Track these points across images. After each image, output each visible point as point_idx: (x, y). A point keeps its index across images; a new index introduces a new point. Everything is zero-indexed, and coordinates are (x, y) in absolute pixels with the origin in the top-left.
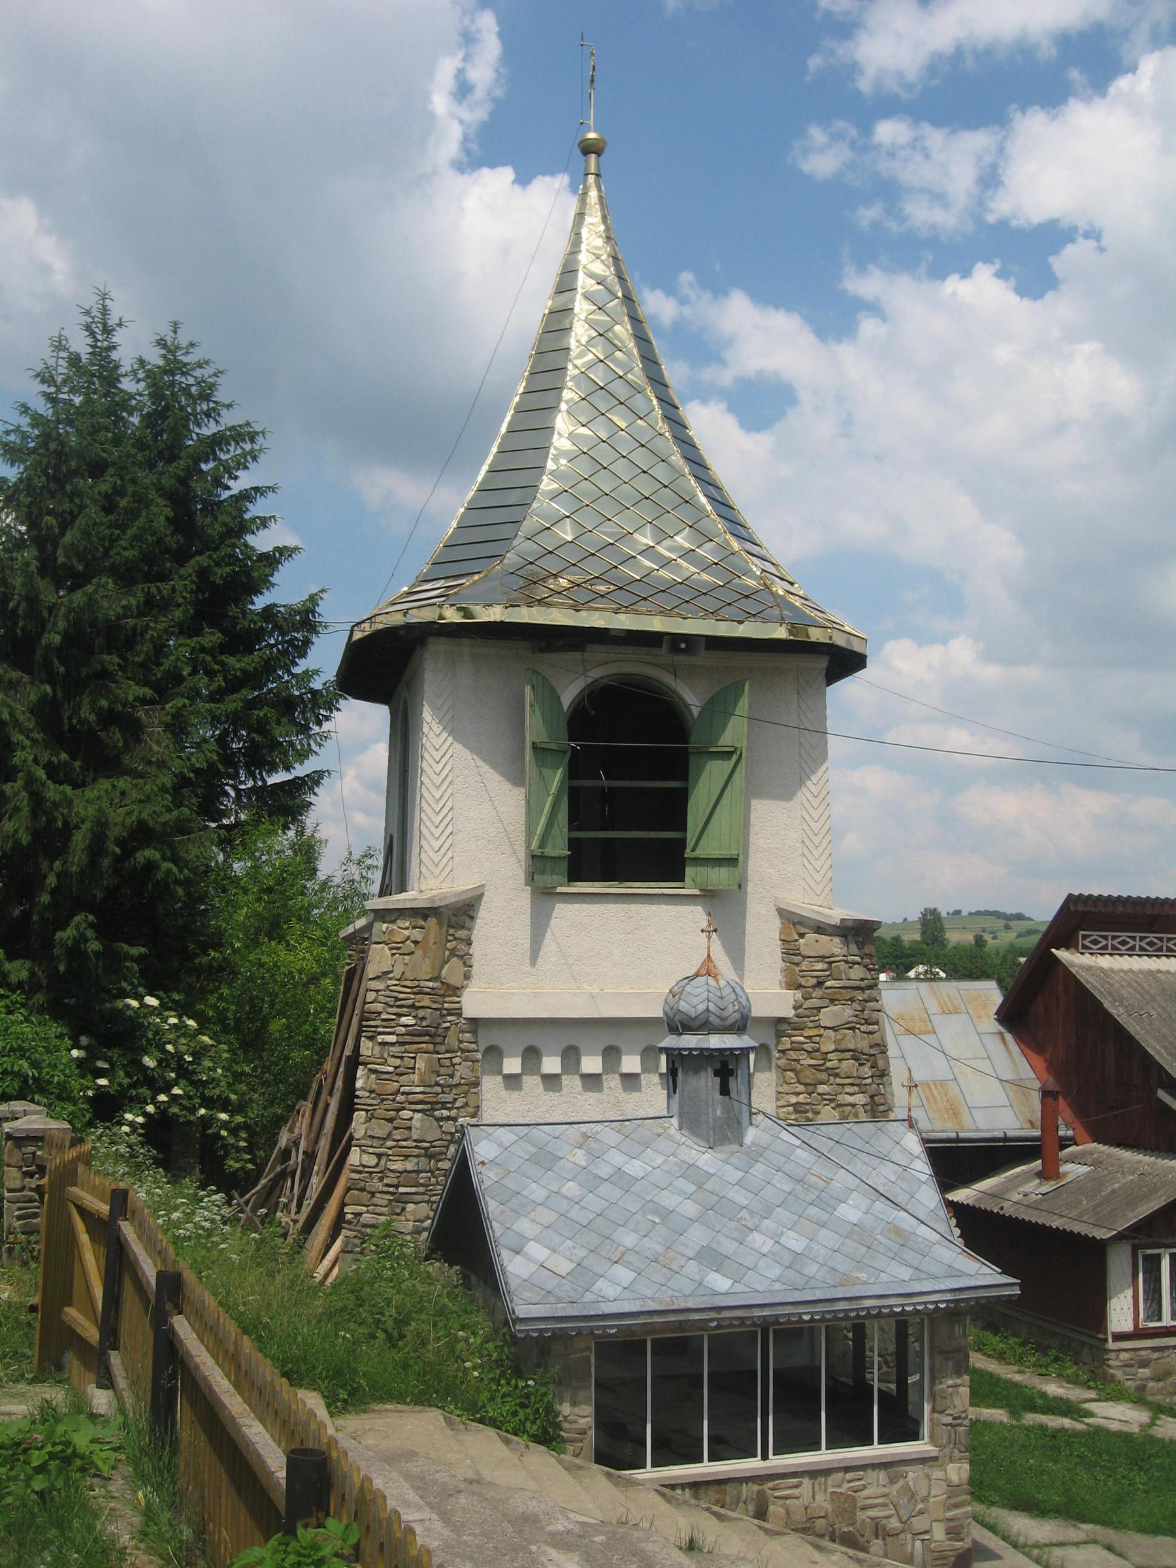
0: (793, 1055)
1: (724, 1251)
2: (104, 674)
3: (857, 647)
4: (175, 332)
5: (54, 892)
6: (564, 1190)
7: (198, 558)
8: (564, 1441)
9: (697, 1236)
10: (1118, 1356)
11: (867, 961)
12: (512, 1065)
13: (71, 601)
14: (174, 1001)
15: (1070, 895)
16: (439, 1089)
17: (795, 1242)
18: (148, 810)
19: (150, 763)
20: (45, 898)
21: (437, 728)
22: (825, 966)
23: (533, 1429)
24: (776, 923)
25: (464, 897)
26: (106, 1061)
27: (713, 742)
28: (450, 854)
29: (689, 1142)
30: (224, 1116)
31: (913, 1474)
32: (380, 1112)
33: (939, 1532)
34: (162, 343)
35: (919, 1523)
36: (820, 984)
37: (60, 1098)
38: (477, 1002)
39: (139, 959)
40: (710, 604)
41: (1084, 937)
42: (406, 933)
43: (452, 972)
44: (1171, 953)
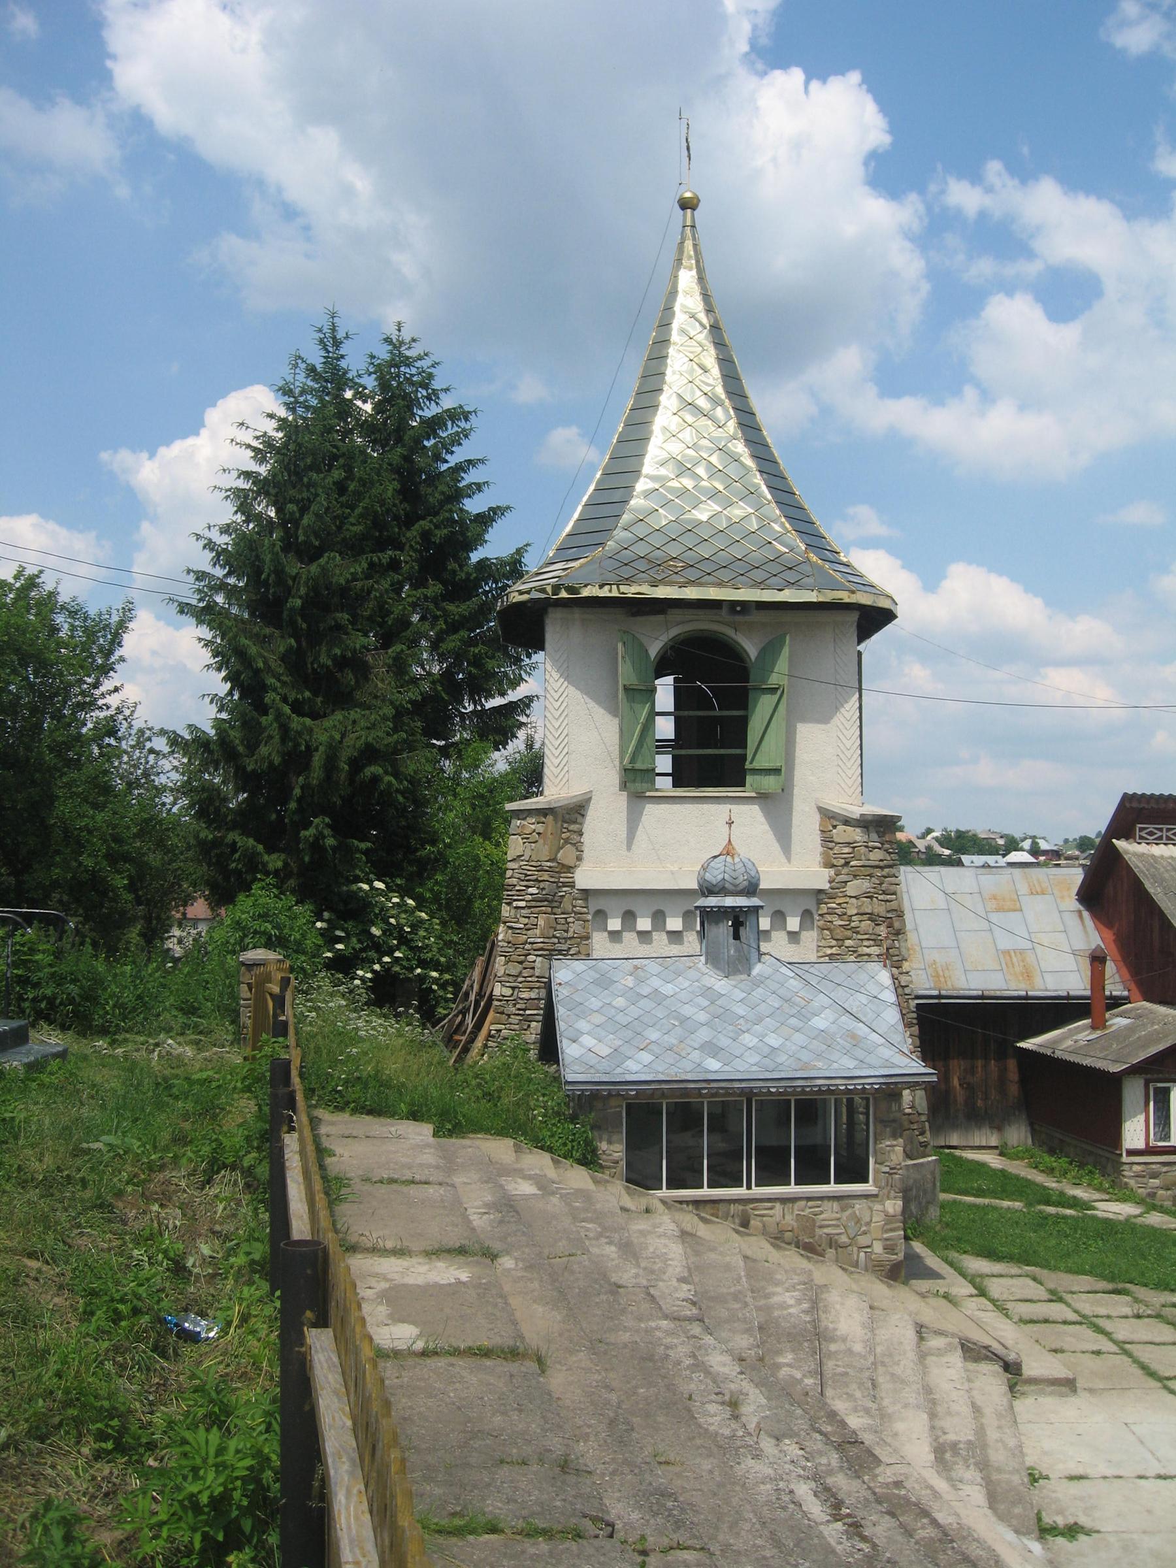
0: (829, 918)
1: (720, 1044)
2: (338, 627)
3: (884, 604)
4: (399, 330)
5: (299, 800)
6: (614, 1003)
7: (422, 522)
8: (602, 1167)
9: (704, 1035)
10: (1132, 1169)
11: (887, 846)
12: (614, 924)
13: (309, 572)
14: (397, 885)
16: (556, 940)
17: (774, 1040)
18: (374, 734)
19: (376, 697)
20: (293, 805)
21: (556, 675)
22: (850, 850)
23: (577, 1155)
24: (817, 817)
25: (574, 800)
26: (343, 930)
27: (764, 682)
28: (566, 769)
29: (711, 973)
30: (435, 974)
31: (859, 1206)
32: (515, 958)
33: (878, 1247)
34: (388, 340)
35: (863, 1240)
36: (847, 864)
37: (297, 952)
38: (585, 878)
39: (366, 852)
40: (758, 575)
41: (1141, 829)
42: (533, 827)
43: (566, 855)
44: (1169, 841)
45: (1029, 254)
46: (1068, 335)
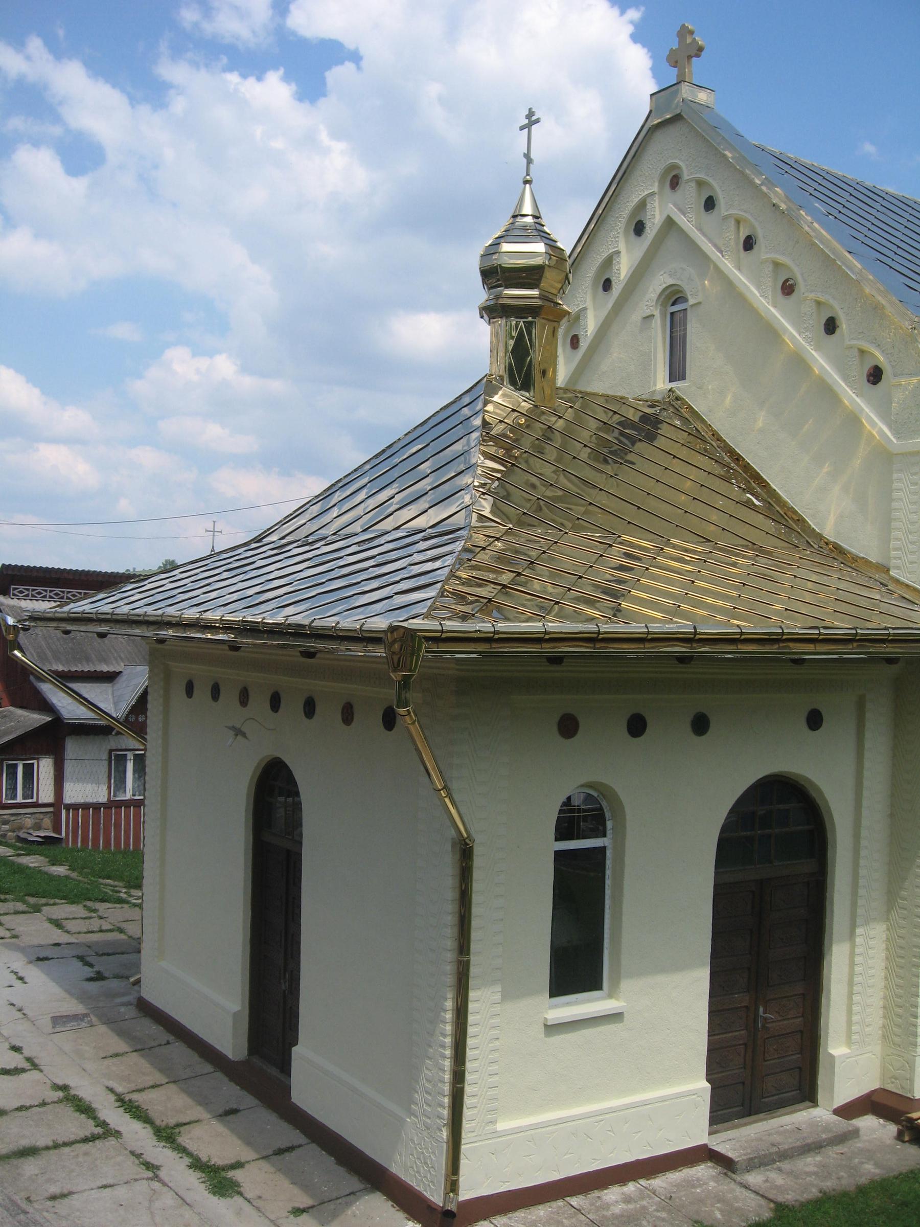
15: (3, 565)
45: (57, 119)
46: (80, 185)
